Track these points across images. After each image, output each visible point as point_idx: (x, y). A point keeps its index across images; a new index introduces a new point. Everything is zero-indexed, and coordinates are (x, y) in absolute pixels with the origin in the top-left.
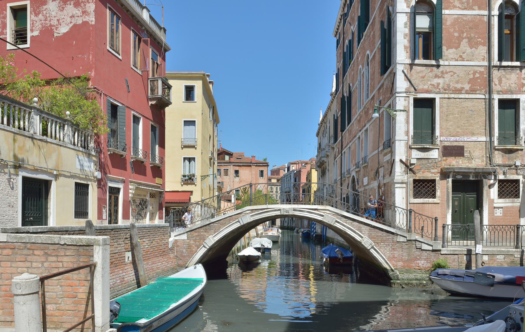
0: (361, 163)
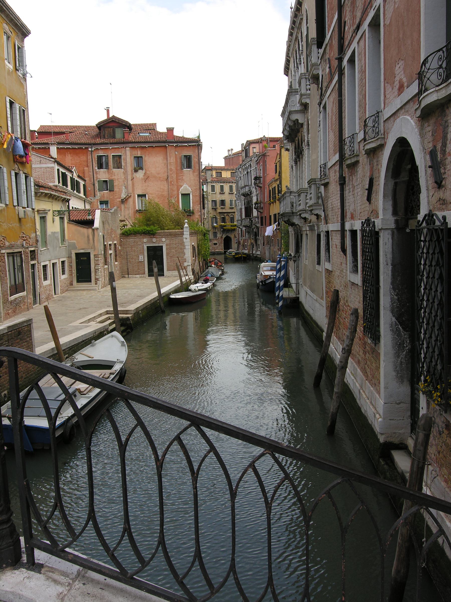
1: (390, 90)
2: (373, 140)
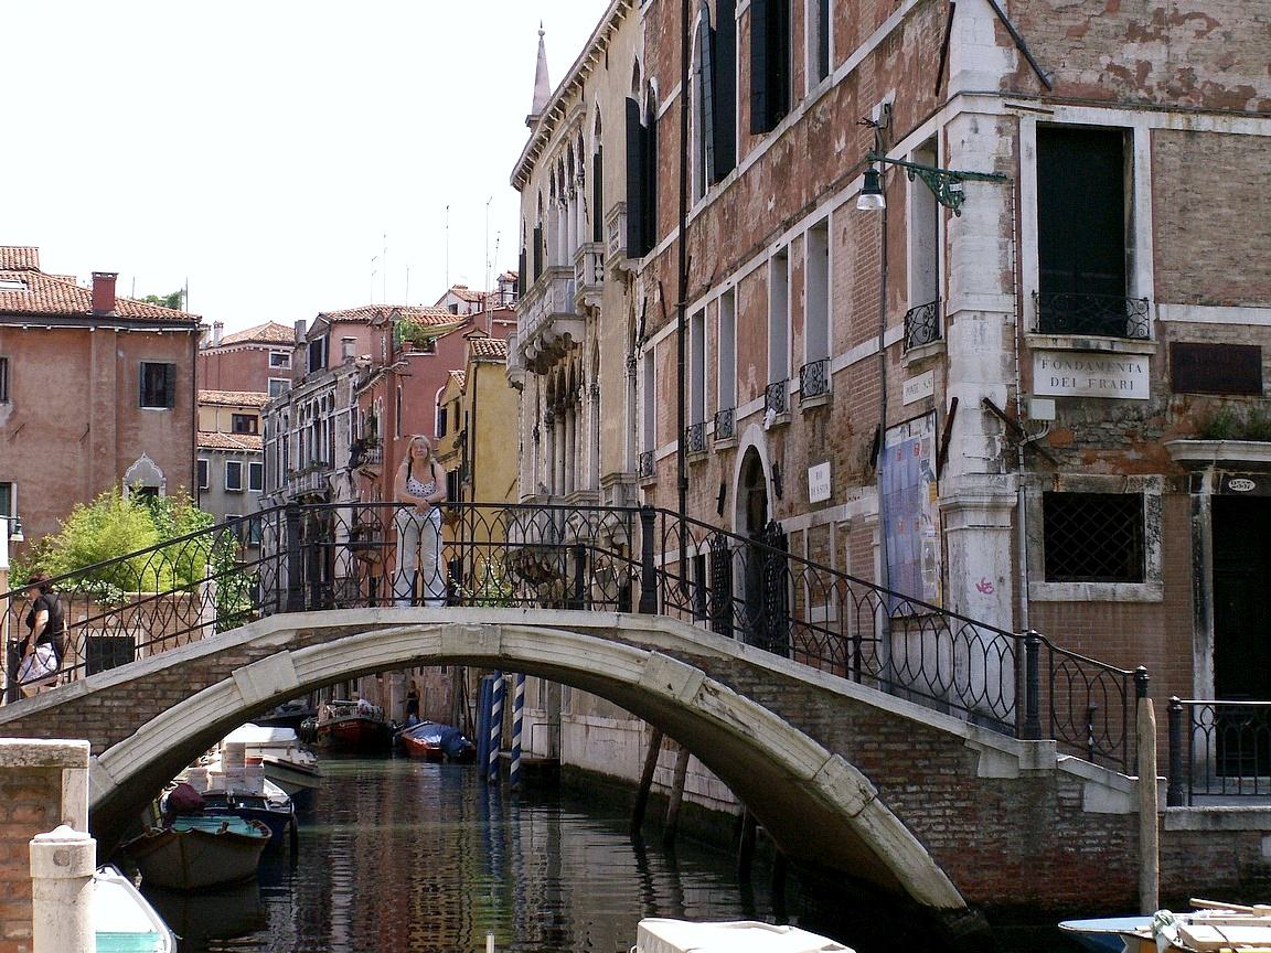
0: (794, 386)
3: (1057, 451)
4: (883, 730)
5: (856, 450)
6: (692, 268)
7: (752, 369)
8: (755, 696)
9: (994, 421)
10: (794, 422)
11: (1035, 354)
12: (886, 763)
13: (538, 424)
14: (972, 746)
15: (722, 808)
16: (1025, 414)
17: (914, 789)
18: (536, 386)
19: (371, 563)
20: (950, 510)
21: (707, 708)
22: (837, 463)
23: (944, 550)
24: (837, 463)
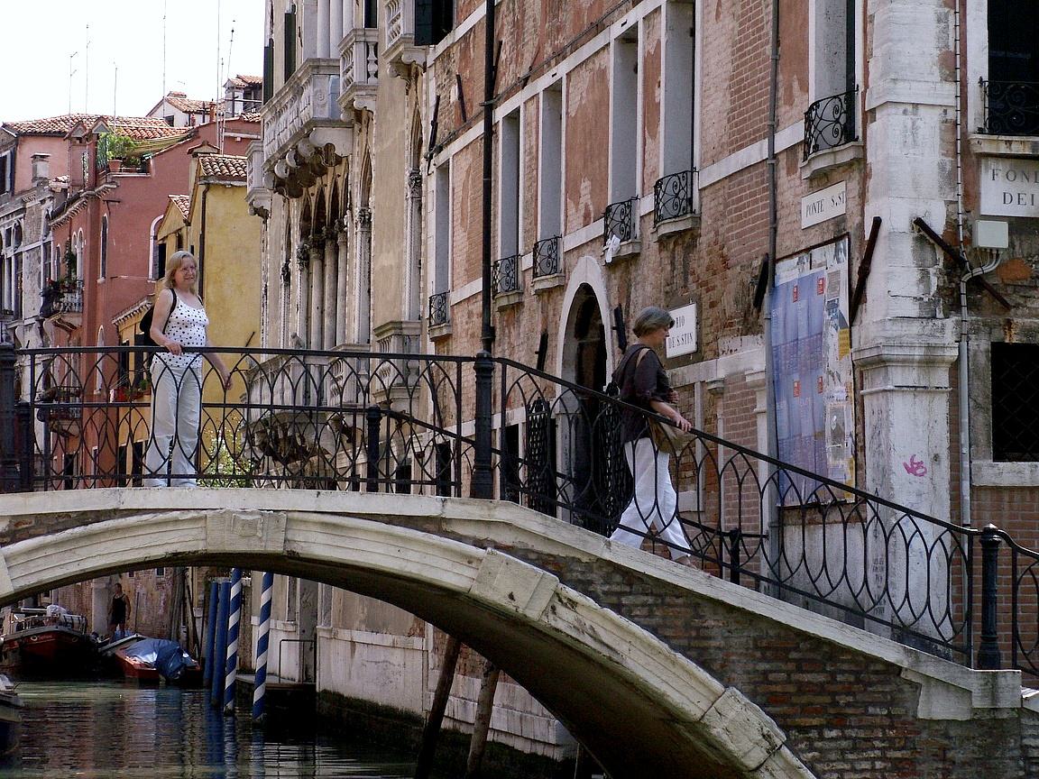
0: (646, 205)
1: (574, 210)
2: (547, 277)
3: (1010, 290)
4: (794, 655)
5: (733, 286)
6: (503, 56)
7: (585, 186)
8: (623, 609)
9: (928, 249)
10: (645, 253)
11: (983, 161)
12: (794, 699)
13: (288, 261)
14: (910, 677)
15: (540, 750)
16: (969, 240)
17: (834, 733)
18: (286, 214)
19: (67, 435)
20: (867, 366)
21: (561, 625)
22: (706, 305)
23: (860, 420)
24: (706, 305)
